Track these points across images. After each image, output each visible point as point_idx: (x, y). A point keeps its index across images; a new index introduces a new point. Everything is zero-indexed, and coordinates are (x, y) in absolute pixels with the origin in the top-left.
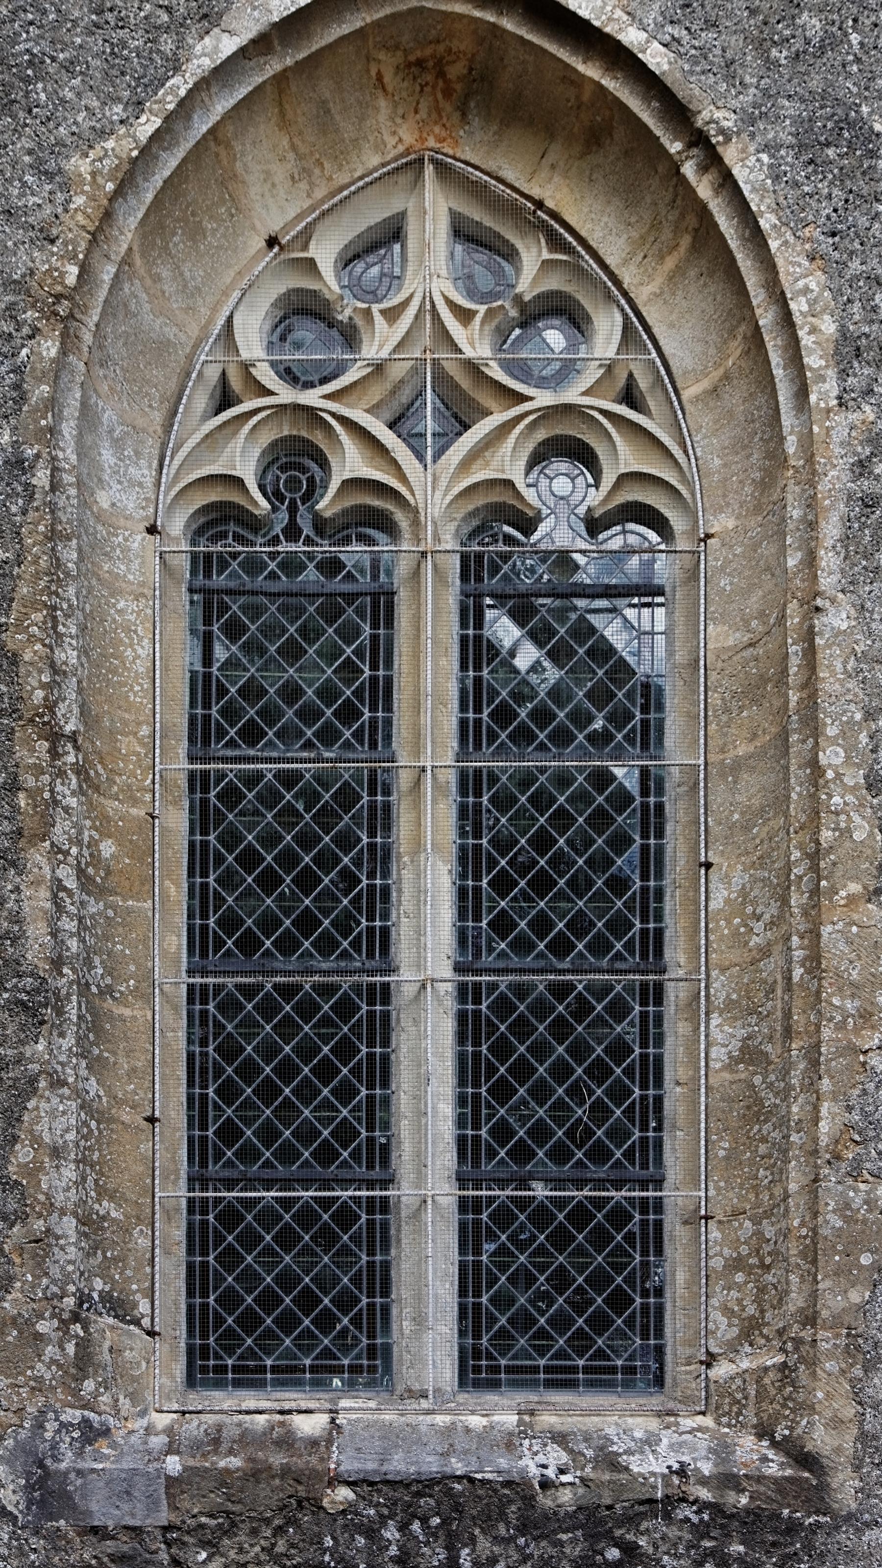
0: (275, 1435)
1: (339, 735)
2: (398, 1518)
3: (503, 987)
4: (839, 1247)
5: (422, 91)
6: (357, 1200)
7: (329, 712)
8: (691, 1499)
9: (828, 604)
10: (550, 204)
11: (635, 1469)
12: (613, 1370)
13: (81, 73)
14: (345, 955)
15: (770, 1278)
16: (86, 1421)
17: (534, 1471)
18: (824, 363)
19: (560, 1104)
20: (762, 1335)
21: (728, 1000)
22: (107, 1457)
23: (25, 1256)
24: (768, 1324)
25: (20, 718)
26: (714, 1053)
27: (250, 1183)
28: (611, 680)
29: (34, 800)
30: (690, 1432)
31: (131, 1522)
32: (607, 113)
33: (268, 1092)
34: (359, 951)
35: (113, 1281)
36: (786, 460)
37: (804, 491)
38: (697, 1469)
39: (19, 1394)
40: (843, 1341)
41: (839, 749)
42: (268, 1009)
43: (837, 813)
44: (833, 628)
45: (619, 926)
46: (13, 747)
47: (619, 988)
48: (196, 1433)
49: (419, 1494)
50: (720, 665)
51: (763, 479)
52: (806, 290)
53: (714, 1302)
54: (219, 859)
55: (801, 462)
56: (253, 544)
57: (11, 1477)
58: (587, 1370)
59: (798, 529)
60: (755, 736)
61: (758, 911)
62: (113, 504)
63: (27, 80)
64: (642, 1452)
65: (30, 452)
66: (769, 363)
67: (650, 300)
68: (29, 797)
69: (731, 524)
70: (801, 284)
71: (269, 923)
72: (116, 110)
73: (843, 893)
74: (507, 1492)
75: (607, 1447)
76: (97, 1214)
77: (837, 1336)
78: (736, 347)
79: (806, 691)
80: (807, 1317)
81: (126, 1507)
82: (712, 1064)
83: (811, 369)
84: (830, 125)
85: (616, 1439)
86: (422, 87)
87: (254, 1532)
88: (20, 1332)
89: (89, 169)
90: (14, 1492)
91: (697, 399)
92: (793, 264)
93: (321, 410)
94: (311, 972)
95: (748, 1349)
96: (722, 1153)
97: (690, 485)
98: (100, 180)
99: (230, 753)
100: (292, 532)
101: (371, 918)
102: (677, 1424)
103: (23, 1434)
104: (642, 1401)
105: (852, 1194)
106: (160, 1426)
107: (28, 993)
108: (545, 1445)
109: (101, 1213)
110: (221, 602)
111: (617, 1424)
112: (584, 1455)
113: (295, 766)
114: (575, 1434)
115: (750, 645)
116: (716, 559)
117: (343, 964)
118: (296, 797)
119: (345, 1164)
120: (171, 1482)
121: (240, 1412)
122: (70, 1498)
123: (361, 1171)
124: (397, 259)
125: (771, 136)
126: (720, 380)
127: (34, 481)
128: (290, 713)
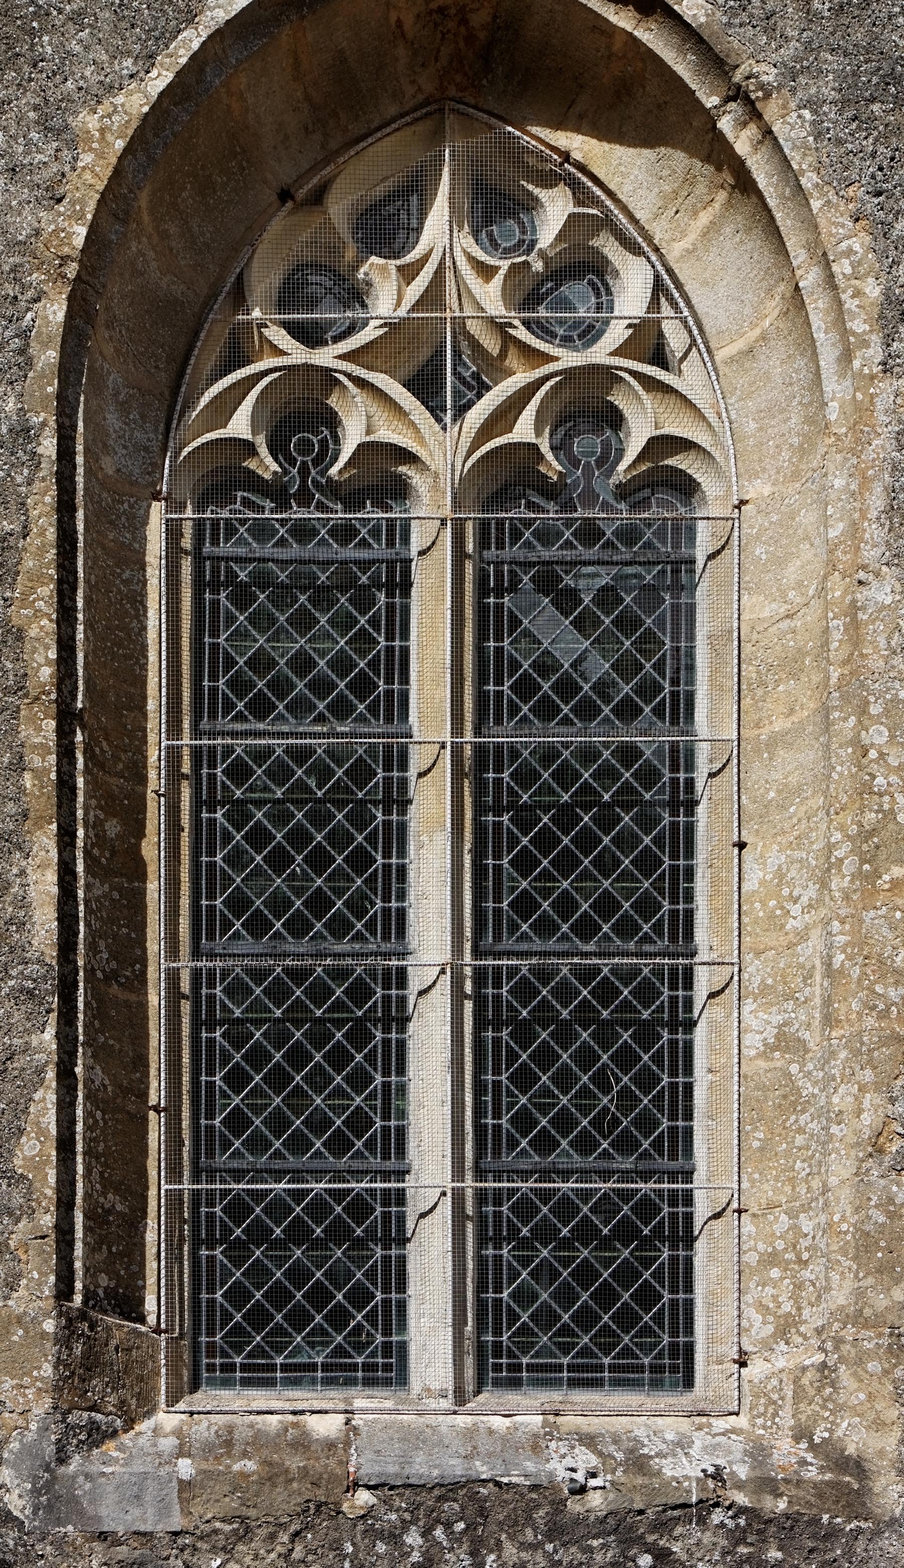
0: (289, 1437)
1: (352, 708)
2: (421, 1523)
3: (524, 971)
4: (883, 1244)
5: (443, 39)
6: (371, 1192)
7: (342, 685)
8: (727, 1503)
9: (871, 577)
10: (576, 155)
11: (668, 1472)
12: (640, 1369)
13: (90, 25)
14: (359, 937)
15: (807, 1274)
16: (92, 1422)
17: (562, 1474)
18: (868, 328)
19: (584, 1092)
20: (800, 1334)
21: (763, 985)
22: (117, 1460)
23: (30, 1253)
24: (805, 1322)
25: (26, 696)
26: (747, 1039)
27: (258, 1175)
28: (640, 651)
29: (41, 781)
30: (723, 1434)
31: (142, 1528)
32: (640, 65)
33: (278, 1079)
34: (374, 933)
35: (118, 1277)
36: (827, 427)
37: (846, 459)
38: (733, 1473)
39: (25, 1396)
40: (885, 1341)
41: (882, 728)
42: (278, 993)
43: (881, 795)
44: (876, 603)
45: (646, 907)
46: (18, 725)
47: (646, 971)
48: (206, 1434)
49: (441, 1499)
50: (755, 636)
51: (801, 445)
52: (850, 252)
53: (748, 1298)
54: (227, 838)
55: (844, 430)
56: (262, 509)
57: (16, 1482)
58: (613, 1368)
59: (841, 500)
60: (792, 711)
61: (795, 894)
62: (119, 470)
63: (32, 33)
64: (675, 1455)
65: (35, 420)
66: (809, 325)
67: (682, 256)
68: (35, 777)
69: (767, 490)
70: (844, 245)
71: (279, 904)
72: (125, 64)
73: (886, 877)
74: (534, 1496)
75: (637, 1450)
76: (103, 1207)
77: (880, 1335)
78: (773, 307)
79: (848, 667)
80: (847, 1316)
81: (136, 1512)
82: (744, 1051)
83: (854, 334)
84: (875, 80)
85: (646, 1442)
86: (443, 34)
87: (272, 1537)
88: (26, 1332)
89: (97, 125)
90: (20, 1496)
91: (732, 359)
92: (837, 224)
93: (336, 371)
94: (322, 955)
95: (783, 1347)
96: (756, 1144)
97: (719, 443)
98: (109, 138)
99: (239, 727)
100: (304, 499)
101: (386, 898)
102: (710, 1425)
103: (30, 1436)
104: (671, 1400)
105: (895, 1188)
106: (168, 1428)
107: (35, 980)
108: (573, 1448)
109: (107, 1206)
110: (229, 570)
111: (646, 1425)
112: (614, 1458)
113: (308, 741)
114: (603, 1435)
115: (787, 616)
116: (752, 527)
117: (357, 946)
118: (307, 773)
119: (358, 1155)
120: (185, 1486)
121: (250, 1412)
122: (78, 1503)
123: (375, 1162)
124: (414, 211)
125: (813, 91)
126: (757, 341)
127: (40, 450)
128: (300, 685)
